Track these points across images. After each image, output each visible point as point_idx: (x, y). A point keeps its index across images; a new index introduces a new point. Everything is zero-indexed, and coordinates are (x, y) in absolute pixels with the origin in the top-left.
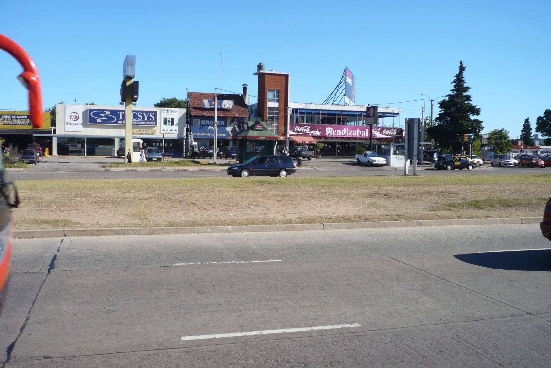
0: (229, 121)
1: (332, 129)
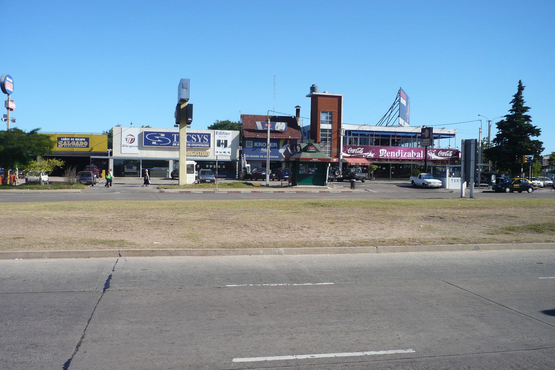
0: (281, 143)
1: (386, 151)
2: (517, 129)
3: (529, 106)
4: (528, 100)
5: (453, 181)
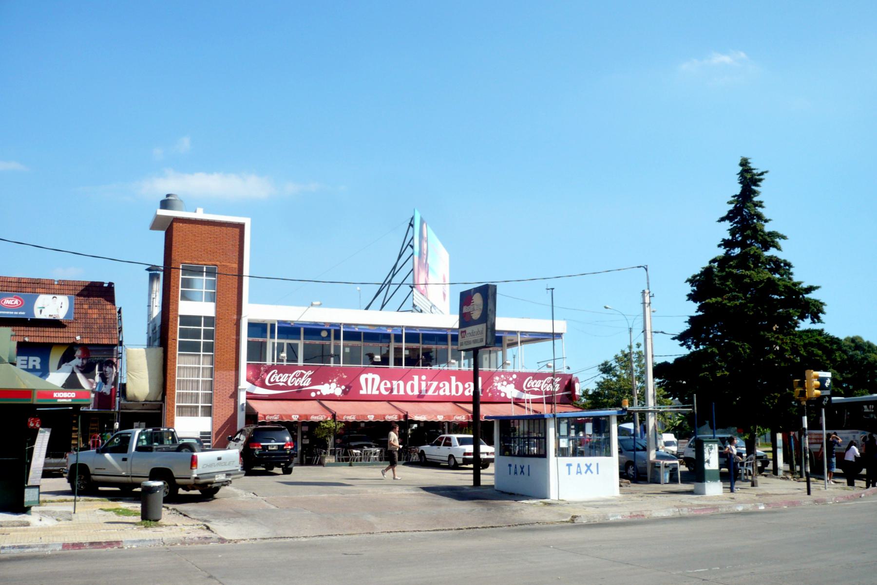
0: (55, 357)
1: (377, 378)
2: (747, 305)
3: (781, 232)
4: (775, 210)
5: (574, 469)
